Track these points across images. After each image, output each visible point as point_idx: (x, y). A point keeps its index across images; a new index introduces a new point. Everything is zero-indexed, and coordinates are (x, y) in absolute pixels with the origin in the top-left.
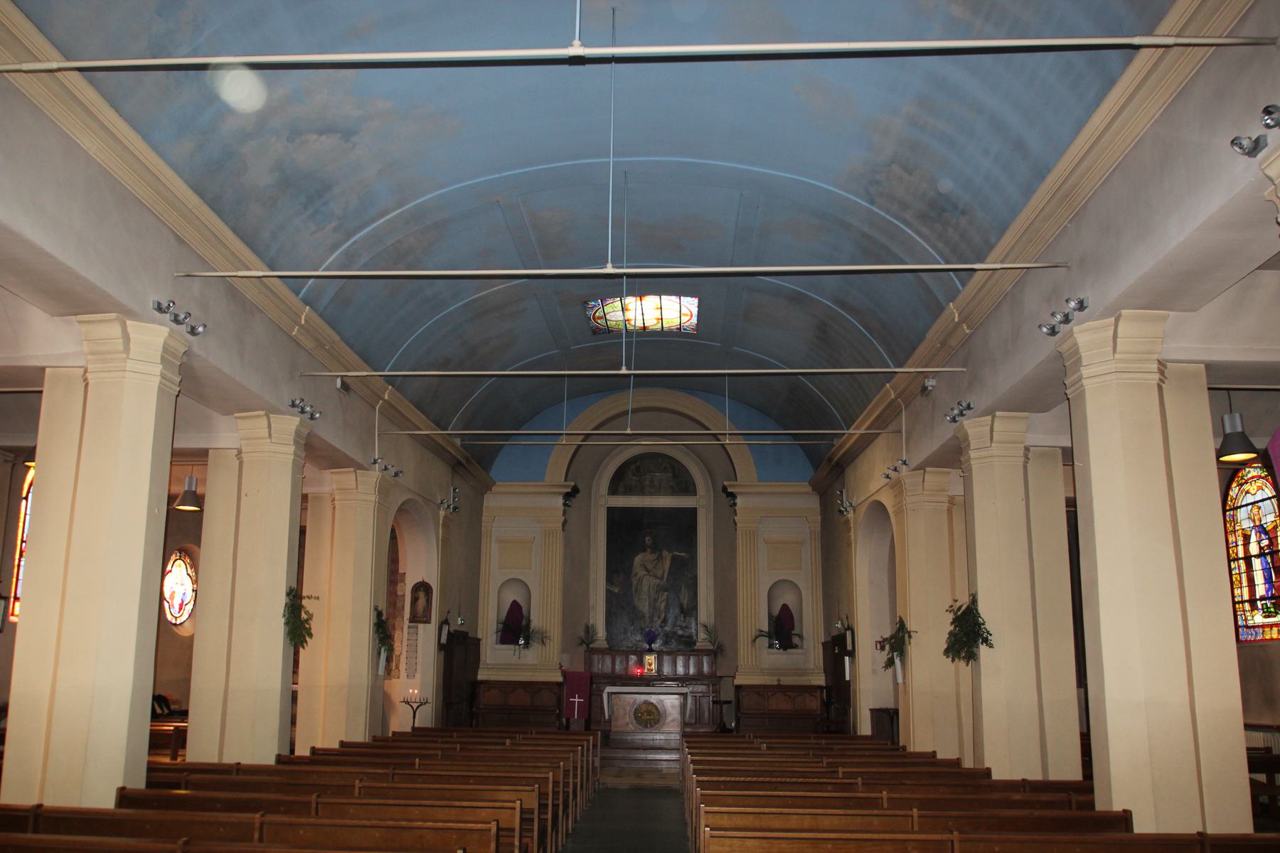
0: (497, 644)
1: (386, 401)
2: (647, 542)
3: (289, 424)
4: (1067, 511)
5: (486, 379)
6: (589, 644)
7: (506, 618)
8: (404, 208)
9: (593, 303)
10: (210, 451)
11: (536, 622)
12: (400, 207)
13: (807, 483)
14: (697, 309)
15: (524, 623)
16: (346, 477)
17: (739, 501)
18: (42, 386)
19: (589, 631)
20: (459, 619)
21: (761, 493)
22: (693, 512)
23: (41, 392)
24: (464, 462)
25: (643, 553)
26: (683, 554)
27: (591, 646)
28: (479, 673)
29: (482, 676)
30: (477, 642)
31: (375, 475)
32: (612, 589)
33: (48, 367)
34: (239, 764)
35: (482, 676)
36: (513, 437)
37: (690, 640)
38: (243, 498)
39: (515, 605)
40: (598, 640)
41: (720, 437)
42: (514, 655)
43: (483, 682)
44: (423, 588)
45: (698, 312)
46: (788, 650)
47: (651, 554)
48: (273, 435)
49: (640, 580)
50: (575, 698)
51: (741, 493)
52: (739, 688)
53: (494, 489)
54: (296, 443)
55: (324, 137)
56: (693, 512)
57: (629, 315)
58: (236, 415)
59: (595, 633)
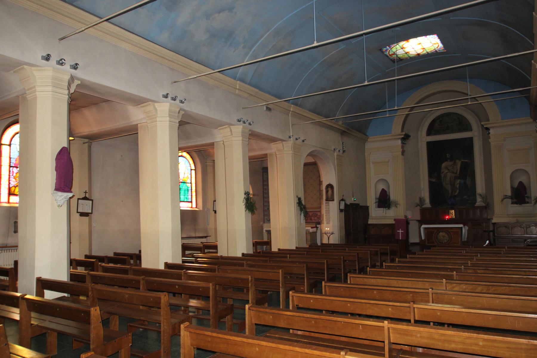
0: (376, 208)
1: (292, 111)
2: (448, 156)
3: (238, 129)
4: (249, 162)
5: (352, 89)
6: (422, 206)
7: (379, 196)
8: (270, 31)
9: (385, 49)
10: (215, 143)
11: (392, 197)
12: (268, 31)
13: (529, 117)
14: (439, 40)
15: (388, 198)
16: (279, 145)
17: (491, 131)
18: (138, 131)
19: (422, 200)
20: (353, 198)
21: (378, 141)
22: (471, 140)
23: (138, 133)
24: (346, 130)
26: (466, 161)
27: (423, 207)
28: (369, 221)
29: (370, 222)
30: (367, 208)
31: (290, 143)
33: (139, 124)
34: (222, 256)
35: (370, 222)
36: (416, 108)
38: (226, 159)
39: (383, 191)
40: (426, 204)
41: (477, 99)
42: (383, 212)
43: (370, 225)
44: (330, 186)
45: (441, 40)
46: (523, 205)
48: (233, 134)
50: (399, 230)
51: (492, 127)
52: (494, 224)
53: (369, 140)
54: (243, 136)
55: (221, 14)
56: (471, 140)
57: (407, 50)
58: (219, 128)
59: (424, 201)
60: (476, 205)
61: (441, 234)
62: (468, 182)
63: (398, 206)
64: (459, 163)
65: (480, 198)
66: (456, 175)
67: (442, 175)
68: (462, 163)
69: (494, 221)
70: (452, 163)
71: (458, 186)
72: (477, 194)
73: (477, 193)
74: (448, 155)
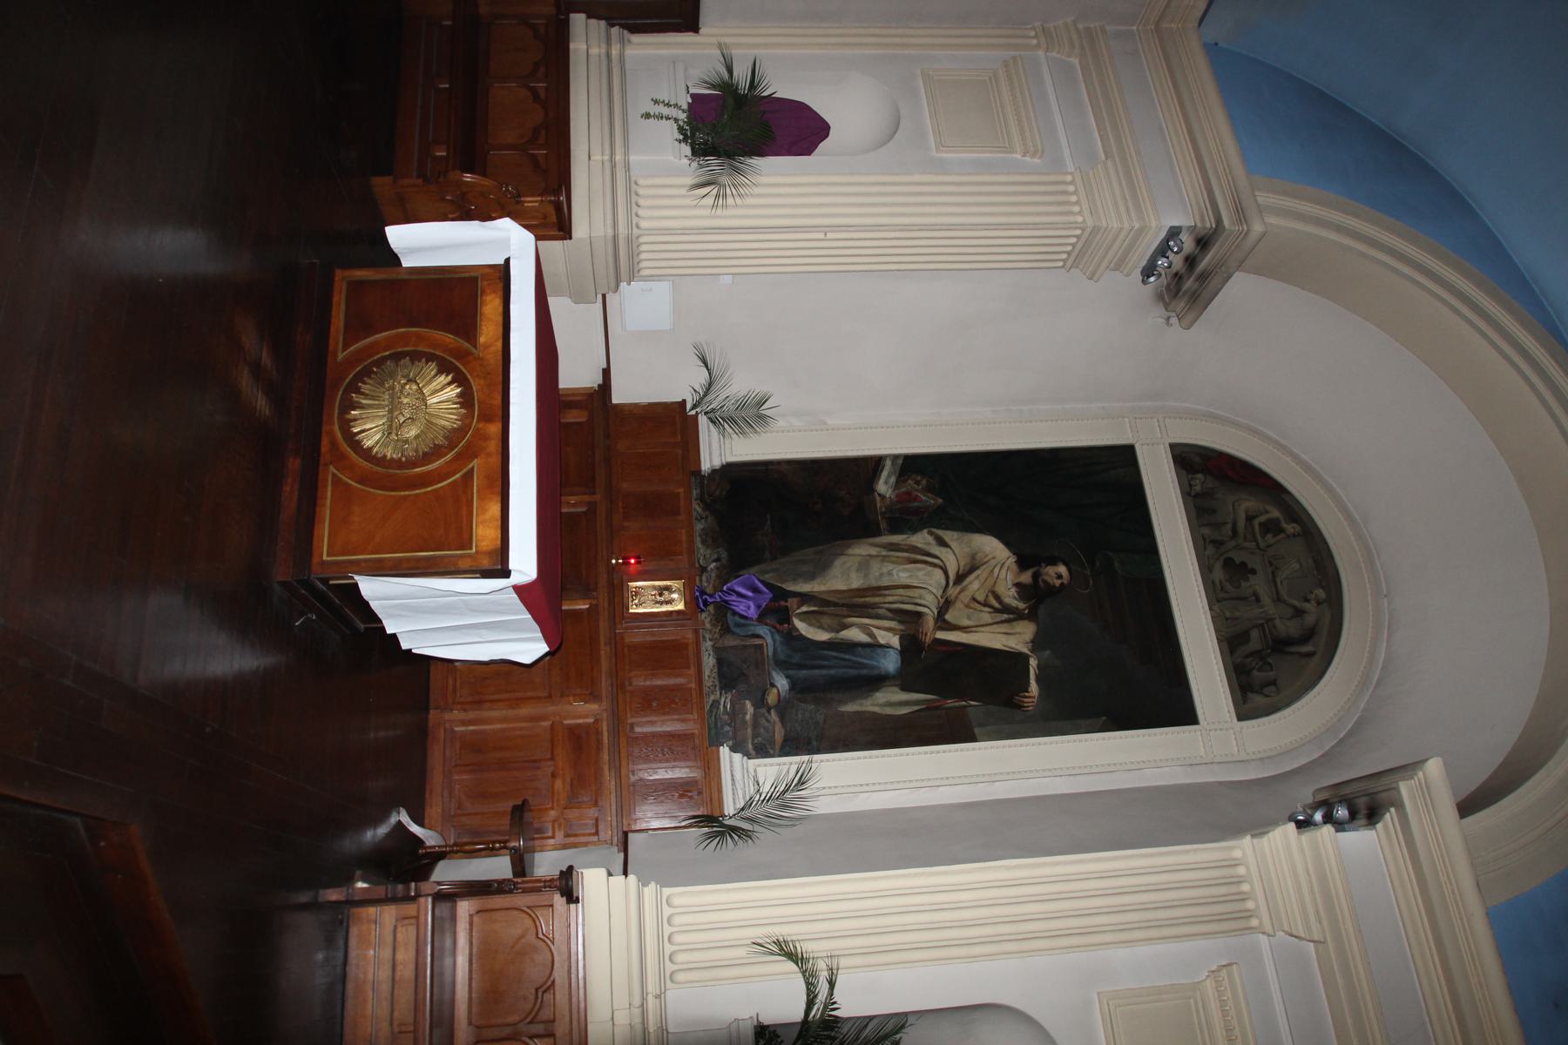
25: (1013, 559)
26: (1034, 688)
32: (885, 474)
37: (611, 22)
42: (656, 102)
47: (1017, 585)
49: (919, 556)
60: (724, 751)
61: (442, 396)
62: (889, 701)
63: (709, 201)
64: (1016, 638)
65: (775, 786)
66: (930, 622)
67: (922, 539)
68: (1018, 660)
69: (593, 881)
70: (1010, 596)
71: (854, 634)
72: (806, 758)
73: (816, 757)
74: (1060, 576)
